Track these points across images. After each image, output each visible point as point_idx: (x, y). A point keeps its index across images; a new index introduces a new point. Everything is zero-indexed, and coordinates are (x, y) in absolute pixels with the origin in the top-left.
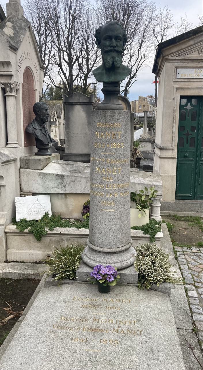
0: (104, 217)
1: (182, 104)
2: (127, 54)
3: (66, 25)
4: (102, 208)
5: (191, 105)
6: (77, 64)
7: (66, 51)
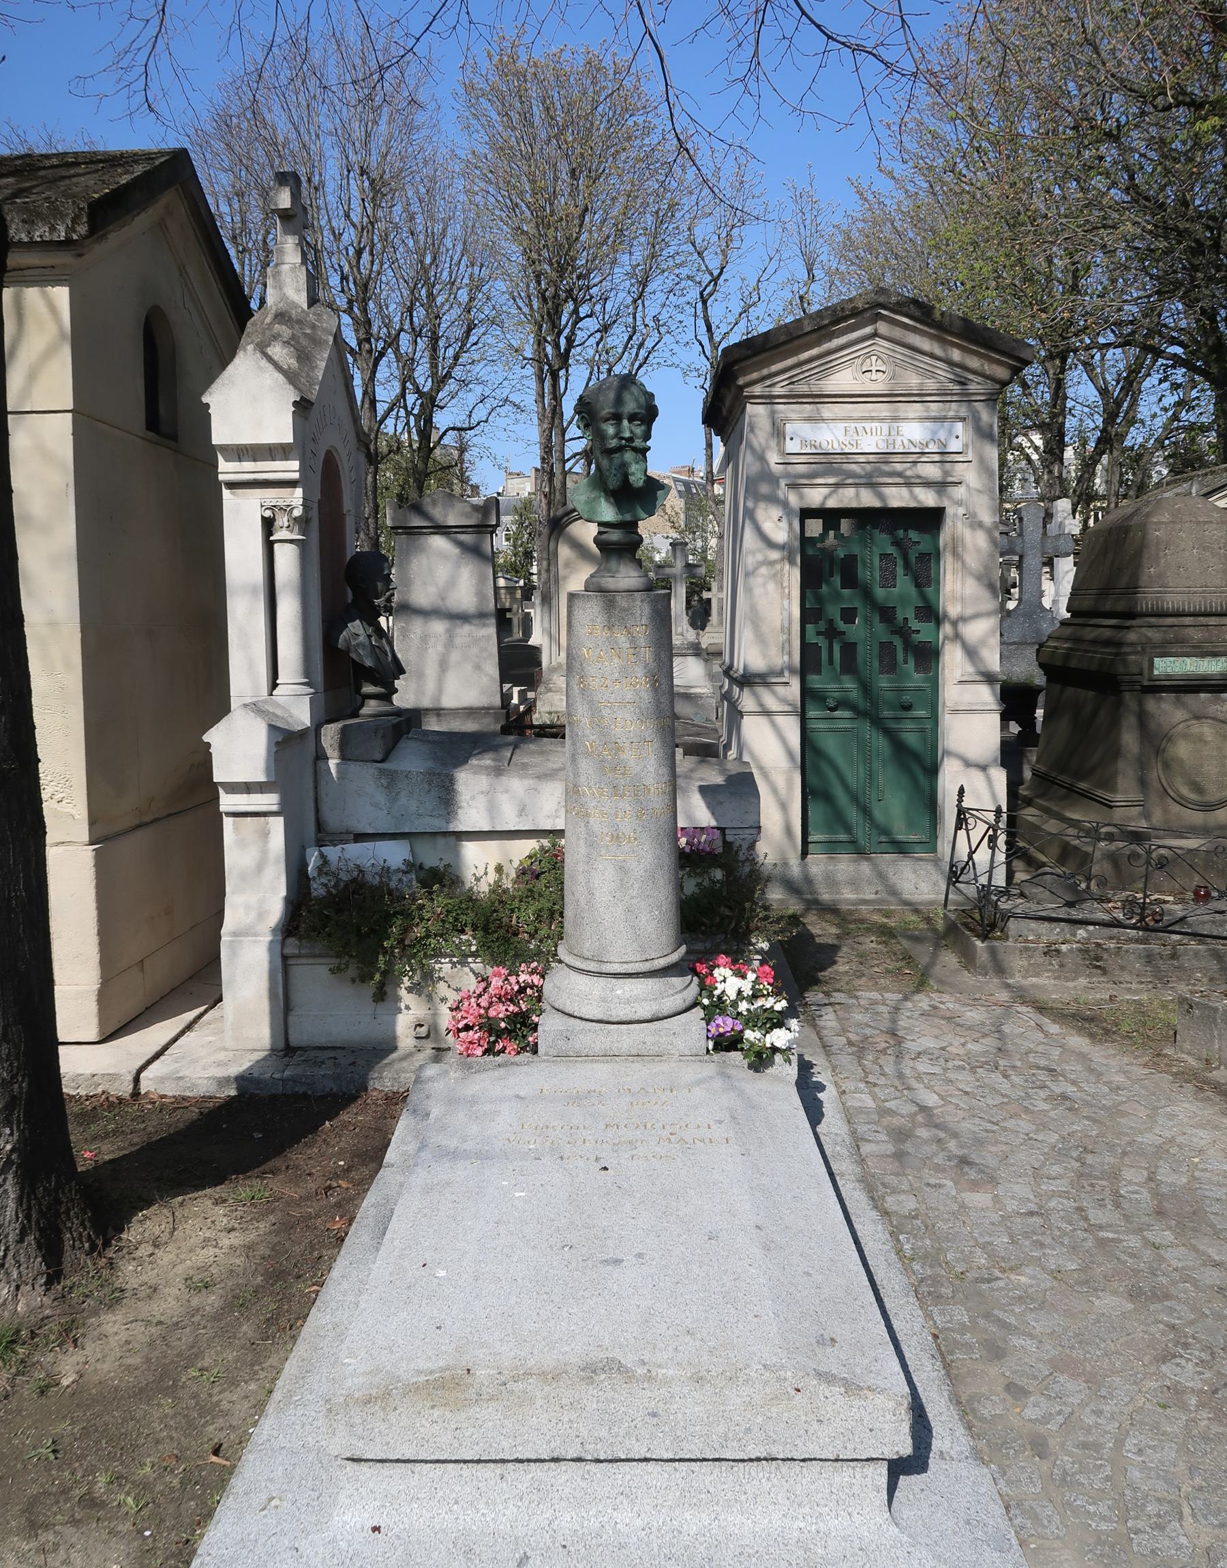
1: (807, 535)
2: (587, 316)
3: (347, 216)
5: (839, 536)
7: (349, 311)
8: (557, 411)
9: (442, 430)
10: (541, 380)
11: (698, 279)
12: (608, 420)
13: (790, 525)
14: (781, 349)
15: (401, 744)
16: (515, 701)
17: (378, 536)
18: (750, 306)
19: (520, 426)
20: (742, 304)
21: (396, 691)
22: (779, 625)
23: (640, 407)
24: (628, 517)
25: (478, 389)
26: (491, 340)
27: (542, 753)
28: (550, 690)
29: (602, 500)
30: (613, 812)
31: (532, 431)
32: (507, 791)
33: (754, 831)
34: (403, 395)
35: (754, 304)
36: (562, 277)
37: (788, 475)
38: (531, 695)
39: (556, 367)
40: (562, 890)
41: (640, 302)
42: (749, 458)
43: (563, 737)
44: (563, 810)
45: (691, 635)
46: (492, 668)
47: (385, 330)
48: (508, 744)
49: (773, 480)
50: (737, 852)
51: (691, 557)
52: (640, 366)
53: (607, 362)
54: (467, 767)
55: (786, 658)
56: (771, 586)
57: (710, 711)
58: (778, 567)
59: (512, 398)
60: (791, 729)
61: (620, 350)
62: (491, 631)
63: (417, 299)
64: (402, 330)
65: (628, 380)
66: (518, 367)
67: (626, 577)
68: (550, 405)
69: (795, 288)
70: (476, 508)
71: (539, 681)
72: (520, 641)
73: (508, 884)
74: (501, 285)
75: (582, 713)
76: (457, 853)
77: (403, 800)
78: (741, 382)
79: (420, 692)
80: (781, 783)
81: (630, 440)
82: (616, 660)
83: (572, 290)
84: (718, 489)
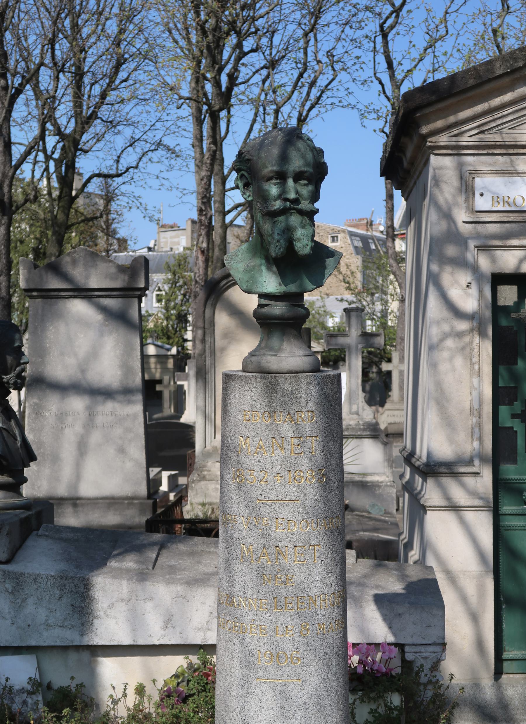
0: (269, 702)
4: (261, 673)
6: (31, 93)
8: (216, 156)
9: (86, 177)
10: (199, 122)
11: (377, 10)
12: (270, 179)
13: (481, 291)
14: (470, 94)
15: (30, 542)
16: (164, 487)
17: (10, 296)
18: (436, 40)
19: (175, 173)
20: (427, 37)
21: (25, 480)
22: (467, 405)
23: (307, 164)
24: (292, 288)
25: (128, 132)
26: (142, 76)
27: (192, 554)
28: (204, 478)
29: (264, 268)
30: (272, 627)
31: (189, 180)
32: (151, 599)
33: (438, 649)
34: (42, 137)
35: (441, 38)
36: (224, 7)
37: (478, 236)
38: (182, 480)
39: (217, 107)
40: (213, 716)
41: (312, 35)
42: (434, 216)
43: (217, 536)
44: (215, 621)
45: (368, 414)
46: (138, 452)
47: (23, 64)
48: (154, 544)
49: (460, 241)
50: (417, 673)
51: (369, 322)
53: (274, 102)
54: (105, 569)
55: (476, 444)
56: (459, 361)
57: (389, 503)
58: (467, 339)
59: (166, 141)
60: (483, 526)
61: (289, 89)
62: (136, 409)
63: (60, 31)
64: (42, 64)
65: (294, 136)
66: (173, 107)
67: (290, 356)
68: (209, 150)
69: (488, 20)
70: (122, 269)
71: (192, 465)
72: (171, 417)
73: (150, 708)
74: (154, 15)
75: (238, 509)
76: (92, 672)
77: (30, 608)
78: (424, 130)
79: (55, 478)
80: (470, 588)
81: (296, 201)
82: (278, 451)
83: (235, 22)
84: (400, 245)
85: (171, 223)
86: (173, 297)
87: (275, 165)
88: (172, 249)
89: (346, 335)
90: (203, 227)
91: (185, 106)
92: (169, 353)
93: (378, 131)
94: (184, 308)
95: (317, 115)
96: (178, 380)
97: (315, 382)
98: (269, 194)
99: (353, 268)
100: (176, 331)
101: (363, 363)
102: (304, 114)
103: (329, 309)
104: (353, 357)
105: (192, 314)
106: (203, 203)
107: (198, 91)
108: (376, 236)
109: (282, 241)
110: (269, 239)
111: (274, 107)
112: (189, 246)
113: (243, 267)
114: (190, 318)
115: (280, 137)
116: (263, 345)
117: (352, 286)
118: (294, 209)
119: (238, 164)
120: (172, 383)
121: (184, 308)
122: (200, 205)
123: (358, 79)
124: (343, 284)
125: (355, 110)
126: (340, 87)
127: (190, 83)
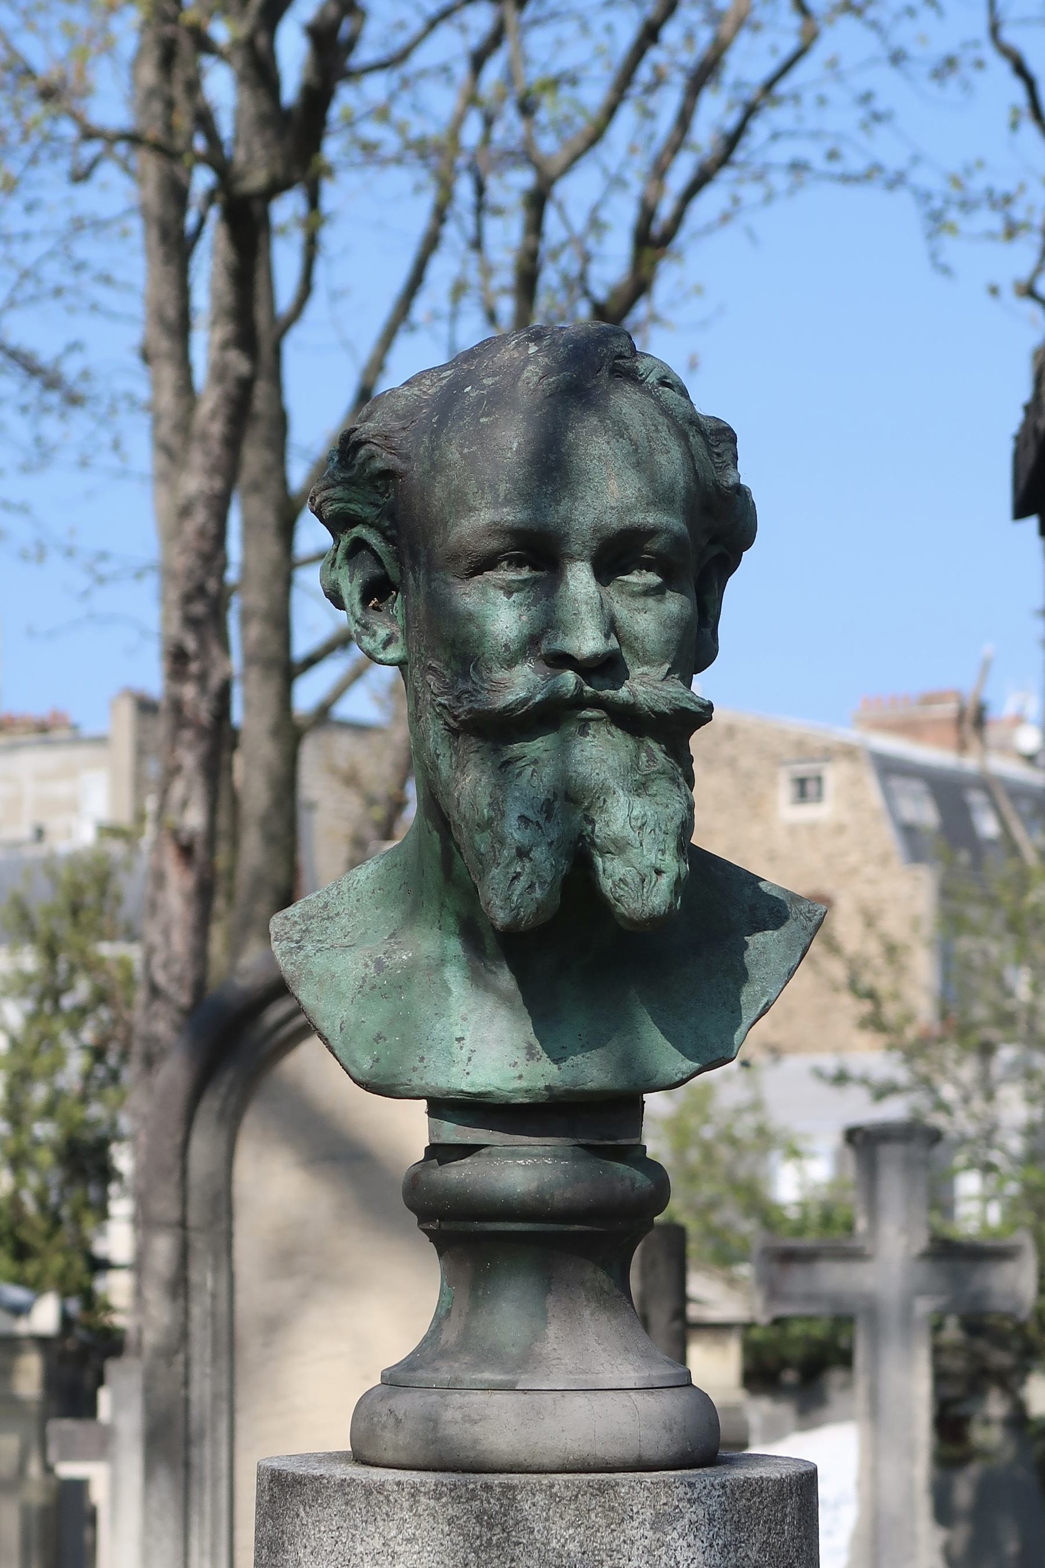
8: (252, 408)
10: (176, 247)
12: (486, 563)
24: (591, 1071)
29: (455, 977)
39: (256, 180)
51: (969, 1184)
52: (701, 180)
53: (525, 155)
61: (594, 94)
67: (578, 1386)
68: (219, 373)
81: (607, 667)
85: (38, 708)
86: (46, 1059)
87: (507, 501)
88: (40, 834)
89: (853, 1255)
90: (188, 735)
91: (108, 172)
92: (22, 1327)
93: (1008, 293)
94: (96, 1111)
95: (726, 218)
96: (67, 1456)
97: (693, 1513)
98: (483, 634)
99: (894, 925)
100: (56, 1222)
101: (940, 1377)
102: (666, 209)
103: (782, 1115)
104: (891, 1355)
105: (133, 1138)
106: (192, 622)
107: (170, 105)
108: (1003, 781)
109: (539, 854)
110: (483, 842)
111: (523, 179)
112: (125, 817)
113: (361, 971)
114: (123, 1160)
115: (533, 371)
116: (450, 1336)
117: (891, 1011)
118: (597, 703)
119: (338, 492)
120: (34, 1469)
121: (96, 1111)
122: (175, 628)
123: (915, 50)
124: (846, 1000)
125: (903, 198)
126: (832, 91)
127: (135, 65)
